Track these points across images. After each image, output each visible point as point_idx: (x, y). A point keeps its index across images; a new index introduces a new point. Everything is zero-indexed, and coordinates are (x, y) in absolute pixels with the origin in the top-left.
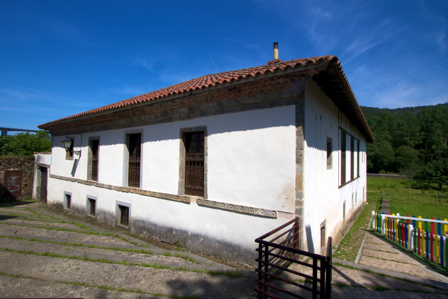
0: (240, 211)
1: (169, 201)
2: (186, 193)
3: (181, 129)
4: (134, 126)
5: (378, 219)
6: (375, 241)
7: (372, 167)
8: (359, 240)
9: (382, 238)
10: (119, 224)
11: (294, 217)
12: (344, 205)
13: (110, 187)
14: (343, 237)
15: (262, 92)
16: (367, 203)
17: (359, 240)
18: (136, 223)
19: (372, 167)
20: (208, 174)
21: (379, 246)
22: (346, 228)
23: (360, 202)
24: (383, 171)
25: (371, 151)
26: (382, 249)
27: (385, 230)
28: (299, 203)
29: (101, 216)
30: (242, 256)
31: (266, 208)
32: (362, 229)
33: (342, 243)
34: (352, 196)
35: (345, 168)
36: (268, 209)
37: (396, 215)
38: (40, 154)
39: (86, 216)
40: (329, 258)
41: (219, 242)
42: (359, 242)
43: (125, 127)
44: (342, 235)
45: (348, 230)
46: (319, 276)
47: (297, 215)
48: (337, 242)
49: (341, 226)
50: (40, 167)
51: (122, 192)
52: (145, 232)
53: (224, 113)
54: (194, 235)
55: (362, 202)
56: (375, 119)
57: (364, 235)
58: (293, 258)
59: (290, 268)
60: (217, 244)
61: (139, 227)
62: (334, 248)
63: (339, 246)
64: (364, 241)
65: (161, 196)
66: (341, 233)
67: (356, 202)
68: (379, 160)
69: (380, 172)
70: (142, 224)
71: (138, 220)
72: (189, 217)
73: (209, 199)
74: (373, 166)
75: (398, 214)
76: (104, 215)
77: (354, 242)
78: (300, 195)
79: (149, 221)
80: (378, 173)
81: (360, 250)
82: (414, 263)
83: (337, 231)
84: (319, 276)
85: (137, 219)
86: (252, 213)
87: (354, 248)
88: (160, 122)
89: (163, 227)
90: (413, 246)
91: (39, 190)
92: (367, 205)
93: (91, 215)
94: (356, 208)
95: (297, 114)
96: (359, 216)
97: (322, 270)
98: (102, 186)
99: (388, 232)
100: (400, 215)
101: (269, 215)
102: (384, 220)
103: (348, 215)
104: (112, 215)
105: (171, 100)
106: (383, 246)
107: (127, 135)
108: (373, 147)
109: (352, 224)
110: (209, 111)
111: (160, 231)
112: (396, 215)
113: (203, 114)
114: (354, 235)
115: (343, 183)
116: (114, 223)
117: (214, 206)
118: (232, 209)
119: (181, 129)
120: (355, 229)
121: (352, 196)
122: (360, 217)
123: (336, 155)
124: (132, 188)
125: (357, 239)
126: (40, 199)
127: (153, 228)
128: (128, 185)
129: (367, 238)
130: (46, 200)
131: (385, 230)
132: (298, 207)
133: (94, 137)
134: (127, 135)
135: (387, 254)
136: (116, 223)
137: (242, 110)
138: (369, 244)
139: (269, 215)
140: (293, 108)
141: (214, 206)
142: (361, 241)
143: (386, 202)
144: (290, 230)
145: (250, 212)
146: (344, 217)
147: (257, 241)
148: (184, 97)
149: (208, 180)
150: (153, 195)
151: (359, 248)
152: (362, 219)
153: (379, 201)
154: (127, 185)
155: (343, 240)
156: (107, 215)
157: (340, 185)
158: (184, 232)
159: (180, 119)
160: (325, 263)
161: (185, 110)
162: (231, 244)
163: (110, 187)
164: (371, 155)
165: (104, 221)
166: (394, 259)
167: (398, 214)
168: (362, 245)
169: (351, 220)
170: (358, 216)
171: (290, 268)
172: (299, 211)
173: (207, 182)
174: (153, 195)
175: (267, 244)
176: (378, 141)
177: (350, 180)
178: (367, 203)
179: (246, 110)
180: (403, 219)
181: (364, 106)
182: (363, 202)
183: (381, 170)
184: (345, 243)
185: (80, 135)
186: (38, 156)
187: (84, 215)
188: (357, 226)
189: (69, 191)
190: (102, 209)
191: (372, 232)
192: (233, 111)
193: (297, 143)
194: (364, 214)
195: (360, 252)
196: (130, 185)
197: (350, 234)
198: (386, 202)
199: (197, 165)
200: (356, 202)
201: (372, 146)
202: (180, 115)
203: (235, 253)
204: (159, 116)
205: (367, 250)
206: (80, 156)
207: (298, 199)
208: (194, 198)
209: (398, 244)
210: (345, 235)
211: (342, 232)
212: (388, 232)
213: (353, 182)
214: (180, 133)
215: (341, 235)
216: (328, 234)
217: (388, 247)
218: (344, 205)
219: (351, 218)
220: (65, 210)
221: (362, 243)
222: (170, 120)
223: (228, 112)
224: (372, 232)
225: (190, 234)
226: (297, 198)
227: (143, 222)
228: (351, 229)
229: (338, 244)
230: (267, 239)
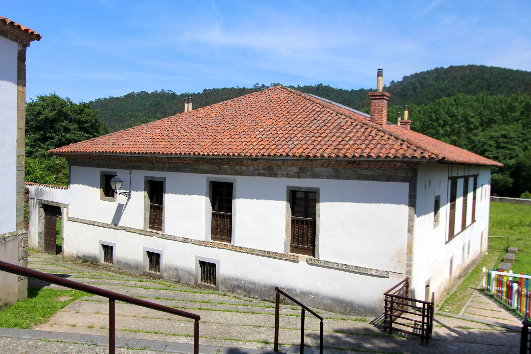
0: (355, 271)
1: (273, 259)
2: (292, 251)
3: (288, 187)
4: (222, 174)
5: (489, 276)
6: (482, 301)
7: (511, 185)
8: (465, 299)
9: (491, 297)
10: (199, 282)
11: (405, 278)
12: (451, 261)
13: (185, 240)
14: (448, 296)
15: (379, 168)
16: (487, 253)
17: (465, 299)
18: (227, 281)
19: (511, 185)
20: (320, 235)
21: (484, 305)
22: (453, 286)
23: (476, 252)
24: (527, 193)
25: (511, 158)
26: (487, 308)
27: (494, 289)
28: (409, 265)
29: (171, 272)
30: (355, 310)
31: (379, 269)
32: (471, 288)
33: (446, 302)
34: (463, 248)
35: (454, 220)
36: (382, 269)
37: (508, 272)
38: (42, 187)
39: (144, 272)
40: (432, 303)
41: (331, 299)
42: (464, 301)
43: (208, 173)
44: (448, 294)
45: (455, 289)
46: (426, 321)
47: (407, 276)
48: (441, 301)
49: (446, 285)
50: (43, 204)
51: (205, 246)
52: (240, 291)
53: (339, 179)
54: (304, 292)
55: (479, 252)
56: (522, 101)
57: (472, 294)
58: (403, 309)
59: (402, 316)
60: (329, 300)
61: (231, 285)
62: (437, 306)
63: (443, 304)
64: (470, 300)
65: (263, 254)
66: (446, 291)
67: (468, 254)
68: (524, 174)
69: (523, 195)
70: (235, 283)
71: (230, 278)
72: (298, 275)
73: (321, 259)
74: (513, 184)
75: (511, 271)
76: (176, 272)
77: (459, 301)
78: (410, 259)
79: (245, 279)
80: (519, 197)
81: (464, 308)
82: (513, 320)
83: (442, 289)
84: (426, 321)
85: (228, 276)
86: (366, 272)
87: (458, 307)
88: (260, 175)
89: (264, 286)
90: (516, 305)
91: (42, 236)
92: (486, 256)
93: (151, 271)
94: (468, 261)
95: (410, 191)
96: (471, 272)
97: (428, 317)
98: (172, 238)
99: (497, 290)
100: (514, 273)
101: (383, 275)
102: (494, 278)
103: (456, 272)
104: (189, 273)
105: (281, 159)
106: (488, 305)
107: (210, 182)
108: (515, 149)
109: (461, 281)
110: (322, 174)
111: (261, 289)
112: (508, 272)
113: (315, 176)
114: (461, 294)
115: (452, 235)
116: (194, 281)
117: (327, 265)
118: (346, 269)
119: (288, 187)
120: (463, 288)
121: (463, 248)
122: (472, 273)
123: (444, 210)
124: (220, 242)
125: (463, 298)
126: (44, 248)
127: (251, 286)
128: (211, 238)
129: (474, 298)
130: (59, 249)
131: (494, 289)
132: (408, 269)
133: (154, 177)
134: (210, 182)
135: (491, 312)
136: (196, 280)
137: (359, 178)
138: (475, 303)
139: (383, 275)
140: (406, 185)
141: (327, 265)
142: (467, 300)
143: (513, 252)
144: (403, 287)
145: (364, 272)
146: (451, 274)
147: (384, 294)
148: (298, 160)
149: (320, 241)
150: (252, 252)
151: (463, 306)
152: (474, 276)
153: (504, 250)
154: (209, 239)
155: (448, 299)
156: (179, 272)
157: (447, 240)
158: (292, 290)
159: (287, 176)
160: (428, 310)
161: (295, 169)
162: (344, 300)
163: (185, 240)
164: (511, 164)
165: (175, 278)
166: (495, 316)
167: (511, 271)
168: (467, 304)
169: (460, 277)
170: (470, 271)
171: (402, 316)
172: (409, 272)
173: (318, 242)
174: (252, 252)
175: (392, 296)
176: (524, 140)
177: (460, 230)
178: (487, 253)
179: (362, 180)
180: (515, 277)
181: (507, 68)
182: (481, 252)
183: (524, 192)
184: (450, 302)
185: (129, 170)
186: (37, 190)
187: (140, 272)
188: (466, 283)
189: (108, 241)
190: (172, 265)
191: (482, 291)
192: (348, 178)
193: (409, 216)
194: (478, 269)
195: (463, 310)
196: (213, 238)
197: (456, 293)
198: (513, 252)
199: (301, 224)
200: (468, 254)
201: (513, 149)
202: (288, 173)
203: (348, 309)
204: (261, 170)
205: (471, 308)
206: (129, 198)
207: (409, 262)
208: (303, 257)
209: (504, 303)
210: (451, 293)
211: (447, 291)
212: (497, 290)
213: (465, 231)
214: (287, 191)
215: (446, 293)
216: (432, 290)
217: (493, 305)
218: (451, 261)
219: (460, 274)
220: (103, 264)
221: (468, 302)
222: (275, 175)
223: (343, 178)
224: (482, 291)
225: (298, 291)
226: (408, 261)
227: (237, 280)
228: (459, 287)
229: (443, 302)
230: (391, 293)
